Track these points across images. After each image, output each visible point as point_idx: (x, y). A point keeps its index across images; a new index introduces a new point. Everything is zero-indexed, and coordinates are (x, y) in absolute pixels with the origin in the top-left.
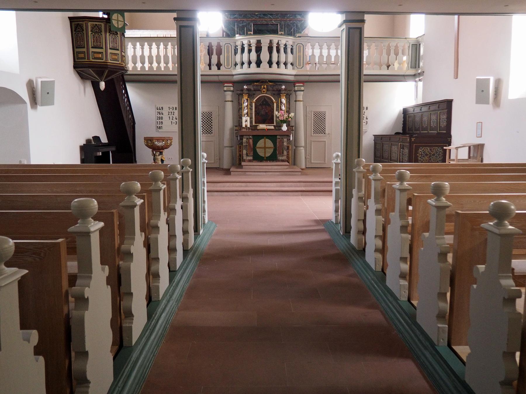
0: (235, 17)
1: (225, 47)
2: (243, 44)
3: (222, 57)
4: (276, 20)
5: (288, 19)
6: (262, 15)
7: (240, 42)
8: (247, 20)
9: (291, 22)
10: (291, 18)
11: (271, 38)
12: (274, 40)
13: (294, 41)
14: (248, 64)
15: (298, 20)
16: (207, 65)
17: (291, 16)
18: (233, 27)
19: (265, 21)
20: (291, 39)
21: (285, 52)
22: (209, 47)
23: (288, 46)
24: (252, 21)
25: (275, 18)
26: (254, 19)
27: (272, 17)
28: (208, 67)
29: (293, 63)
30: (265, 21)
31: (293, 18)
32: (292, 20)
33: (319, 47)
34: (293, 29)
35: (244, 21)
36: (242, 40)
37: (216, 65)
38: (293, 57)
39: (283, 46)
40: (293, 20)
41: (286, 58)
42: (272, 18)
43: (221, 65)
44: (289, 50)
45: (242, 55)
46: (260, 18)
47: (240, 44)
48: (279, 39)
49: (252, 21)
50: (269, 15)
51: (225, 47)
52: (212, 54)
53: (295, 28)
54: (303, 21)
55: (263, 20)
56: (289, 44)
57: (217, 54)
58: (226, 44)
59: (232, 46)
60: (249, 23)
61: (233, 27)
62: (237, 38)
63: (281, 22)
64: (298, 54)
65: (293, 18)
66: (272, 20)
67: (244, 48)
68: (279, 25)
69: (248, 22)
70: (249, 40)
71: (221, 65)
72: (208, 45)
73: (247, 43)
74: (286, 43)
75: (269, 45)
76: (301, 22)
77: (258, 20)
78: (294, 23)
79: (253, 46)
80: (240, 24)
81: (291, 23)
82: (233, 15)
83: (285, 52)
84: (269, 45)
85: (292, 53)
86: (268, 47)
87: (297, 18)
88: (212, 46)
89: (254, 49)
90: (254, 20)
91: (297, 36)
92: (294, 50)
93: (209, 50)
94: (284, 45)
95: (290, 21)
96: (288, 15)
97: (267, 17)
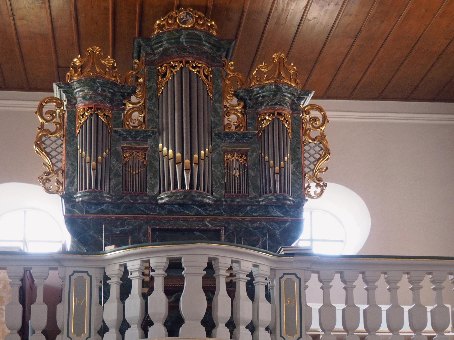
0: (102, 209)
1: (73, 282)
2: (126, 272)
3: (61, 309)
4: (215, 220)
5: (248, 218)
6: (176, 206)
7: (117, 267)
8: (135, 218)
9: (256, 225)
10: (255, 214)
11: (213, 254)
12: (221, 260)
13: (275, 266)
14: (140, 326)
15: (273, 221)
16: (16, 331)
17: (256, 211)
18: (96, 235)
19: (185, 220)
20: (267, 259)
21: (251, 294)
22: (22, 280)
23: (256, 280)
24: (147, 221)
25: (212, 213)
26: (153, 215)
27: (205, 210)
28: (21, 306)
29: (271, 328)
30: (183, 221)
31: (260, 216)
32: (258, 220)
33: (344, 286)
34: (262, 242)
35: (126, 220)
36: (123, 261)
37: (44, 332)
38: (274, 311)
39: (244, 276)
40: (261, 221)
41: (256, 311)
42: (203, 215)
43: (59, 332)
44: (260, 291)
45: (124, 303)
46: (170, 212)
47: (117, 272)
48: (236, 257)
49: (147, 221)
50: (195, 207)
51: (73, 282)
52: (33, 301)
53: (266, 241)
54: (288, 224)
55: (178, 219)
56: (261, 272)
57: (45, 301)
58: (75, 272)
59: (93, 279)
60: (140, 227)
61: (96, 235)
62: (109, 256)
63: (229, 224)
64: (286, 302)
65: (260, 216)
66: (203, 220)
67: (130, 281)
68: (222, 232)
69: (138, 223)
70: (145, 257)
71: (59, 332)
72: (21, 274)
73: (138, 266)
74: (252, 272)
75: (205, 272)
76: (282, 226)
77: (166, 218)
78: (264, 228)
79: (158, 275)
80: (116, 227)
81: (256, 228)
82: (96, 204)
83: (251, 294)
84: (205, 272)
85: (268, 296)
86: (203, 277)
87: (273, 216)
88: (33, 287)
89: (159, 284)
90: (154, 219)
91: (282, 253)
92: (275, 293)
93: (22, 290)
94: (247, 276)
95: (252, 222)
96: (248, 208)
97: (191, 212)
